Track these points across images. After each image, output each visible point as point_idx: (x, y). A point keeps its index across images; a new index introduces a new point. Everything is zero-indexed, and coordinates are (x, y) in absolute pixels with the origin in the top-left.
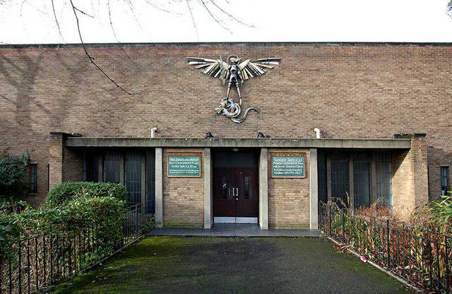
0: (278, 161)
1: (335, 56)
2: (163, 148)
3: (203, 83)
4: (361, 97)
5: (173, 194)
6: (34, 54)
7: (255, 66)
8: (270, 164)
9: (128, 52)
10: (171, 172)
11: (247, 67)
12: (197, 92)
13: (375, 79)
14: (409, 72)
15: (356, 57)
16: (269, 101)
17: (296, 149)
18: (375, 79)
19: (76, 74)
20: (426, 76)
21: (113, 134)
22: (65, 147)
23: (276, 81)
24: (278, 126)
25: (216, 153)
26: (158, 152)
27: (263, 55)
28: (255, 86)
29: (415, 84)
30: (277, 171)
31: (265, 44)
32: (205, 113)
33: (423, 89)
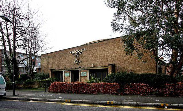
0: (82, 73)
1: (97, 46)
2: (80, 70)
3: (72, 57)
4: (103, 55)
5: (66, 80)
6: (49, 55)
7: (81, 51)
8: (80, 73)
9: (61, 52)
10: (65, 76)
11: (80, 51)
12: (71, 59)
13: (106, 50)
14: (115, 46)
15: (102, 45)
16: (84, 59)
17: (84, 70)
18: (106, 50)
19: (54, 57)
20: (120, 46)
21: (59, 69)
22: (51, 72)
23: (85, 54)
24: (63, 68)
25: (90, 70)
26: (79, 71)
27: (82, 48)
28: (81, 55)
29: (117, 49)
30: (82, 75)
31: (55, 52)
32: (73, 63)
33: (119, 50)
